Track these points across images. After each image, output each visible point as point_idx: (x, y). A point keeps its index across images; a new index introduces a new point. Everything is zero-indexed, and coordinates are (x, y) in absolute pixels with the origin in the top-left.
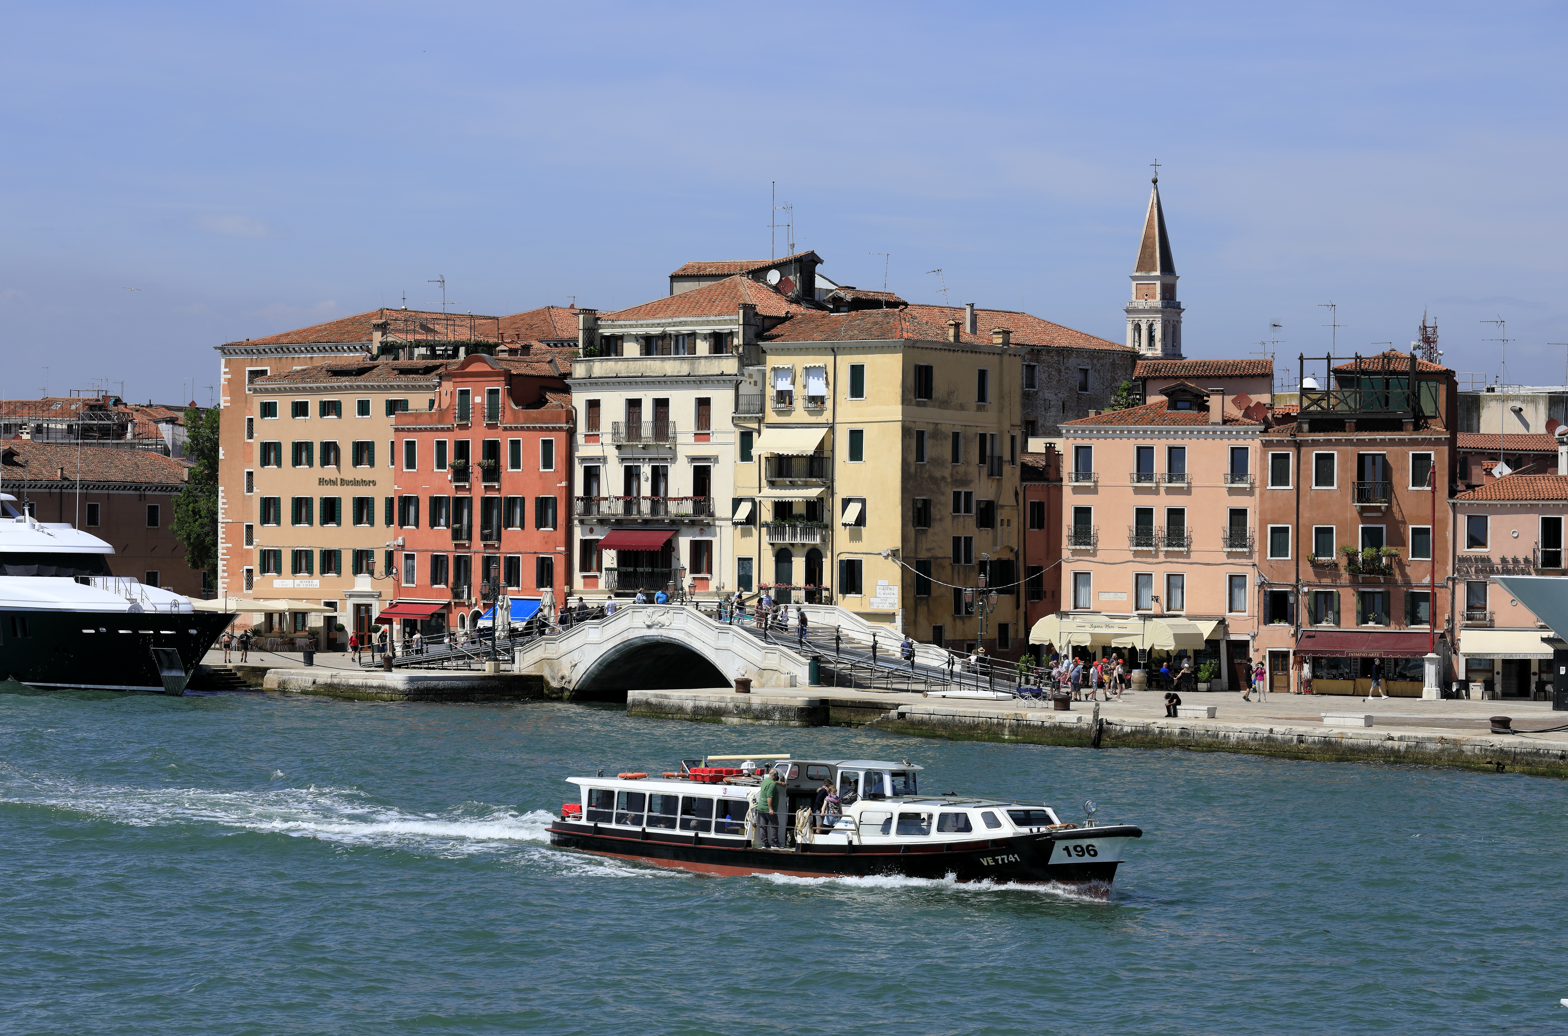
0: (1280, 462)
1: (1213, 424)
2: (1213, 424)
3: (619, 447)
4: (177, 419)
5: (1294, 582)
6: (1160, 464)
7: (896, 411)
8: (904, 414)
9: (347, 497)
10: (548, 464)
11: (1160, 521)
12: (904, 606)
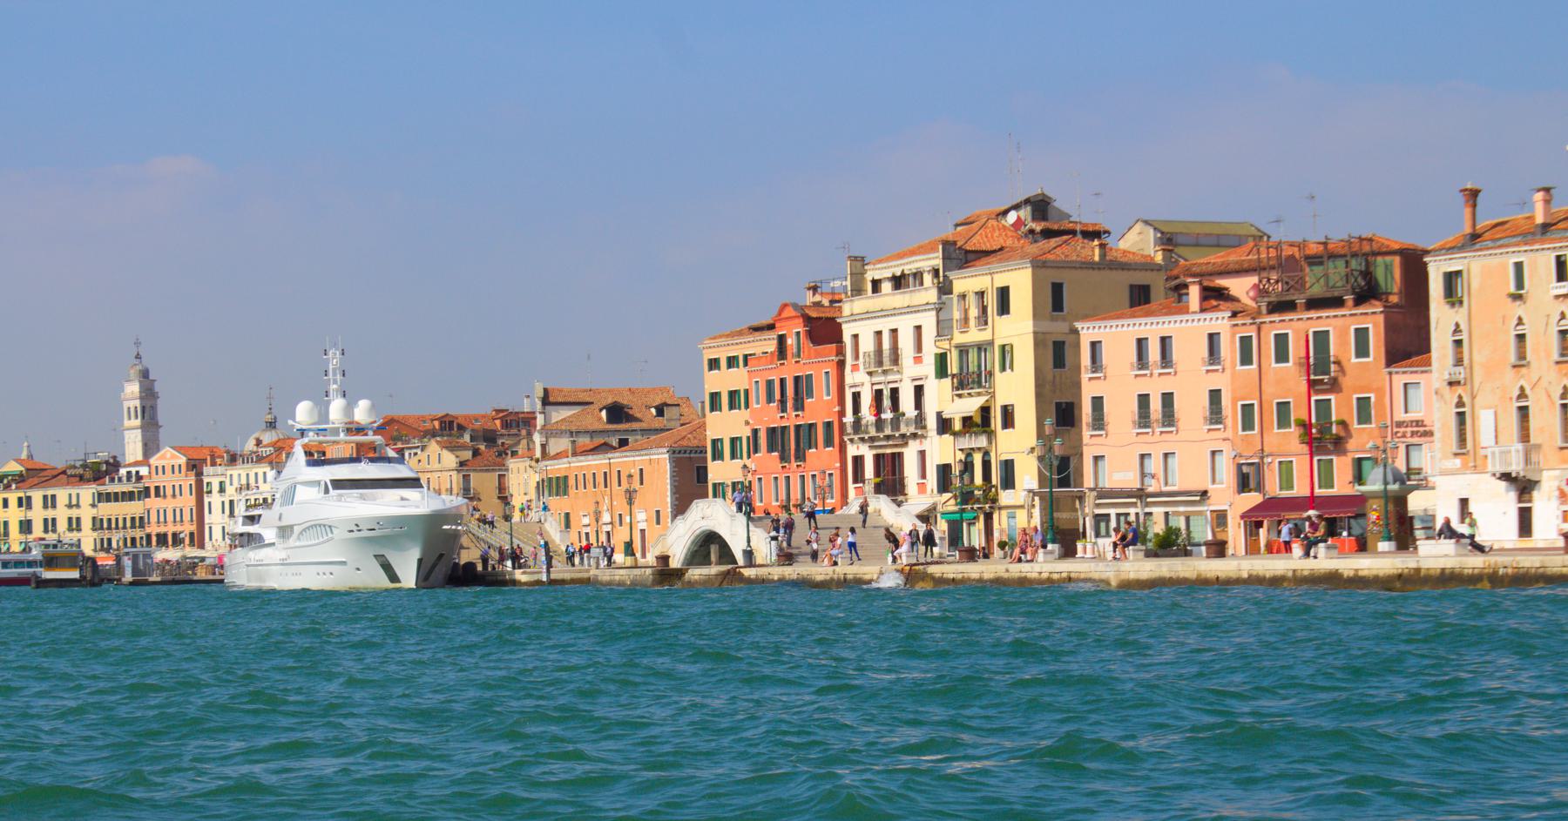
0: (1245, 342)
3: (870, 374)
11: (1156, 405)
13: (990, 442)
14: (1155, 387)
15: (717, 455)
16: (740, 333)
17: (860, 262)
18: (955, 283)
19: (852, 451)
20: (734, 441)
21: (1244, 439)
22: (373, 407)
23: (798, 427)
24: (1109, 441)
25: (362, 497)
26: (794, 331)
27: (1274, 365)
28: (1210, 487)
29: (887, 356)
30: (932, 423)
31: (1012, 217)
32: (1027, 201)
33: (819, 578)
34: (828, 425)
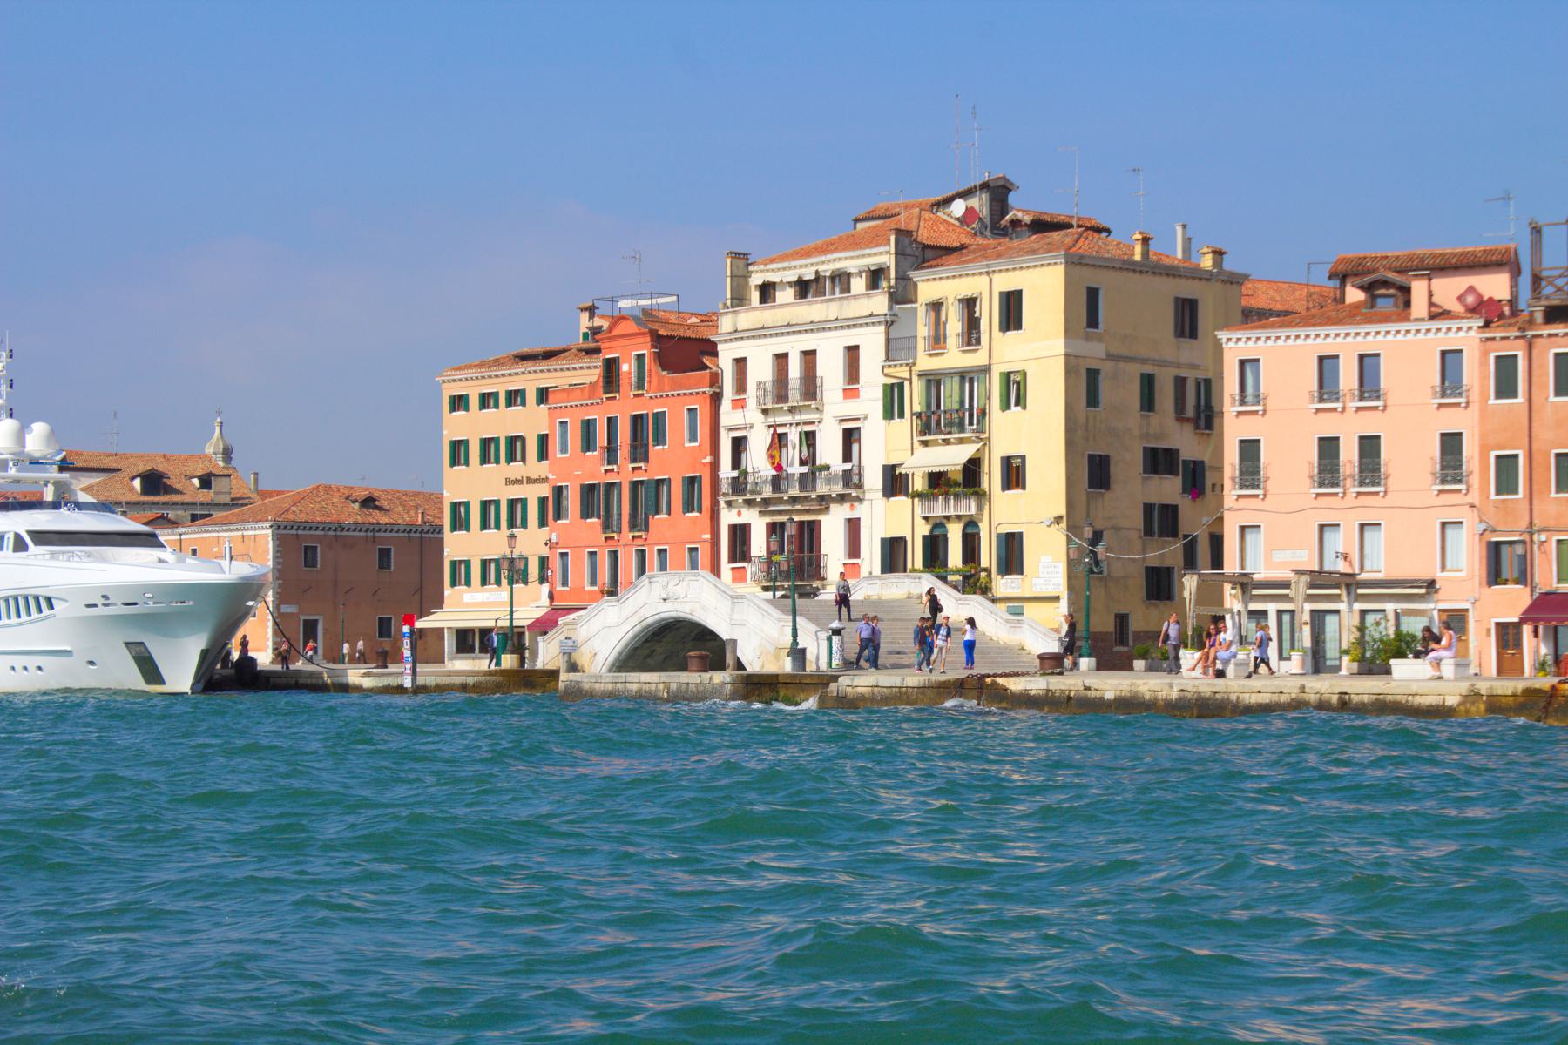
0: (1506, 367)
1: (1417, 320)
2: (1417, 320)
3: (765, 412)
5: (1524, 524)
6: (1348, 377)
7: (1058, 346)
8: (1067, 345)
9: (533, 494)
10: (693, 438)
11: (1349, 454)
12: (1071, 588)
13: (980, 508)
14: (1349, 428)
15: (460, 523)
16: (498, 363)
17: (742, 259)
18: (921, 286)
19: (728, 518)
20: (485, 505)
21: (1499, 506)
22: (53, 435)
23: (635, 485)
24: (1268, 504)
25: (89, 555)
26: (631, 354)
27: (1552, 398)
28: (1439, 575)
29: (795, 385)
30: (873, 480)
31: (958, 208)
32: (985, 186)
33: (1254, 699)
34: (691, 482)
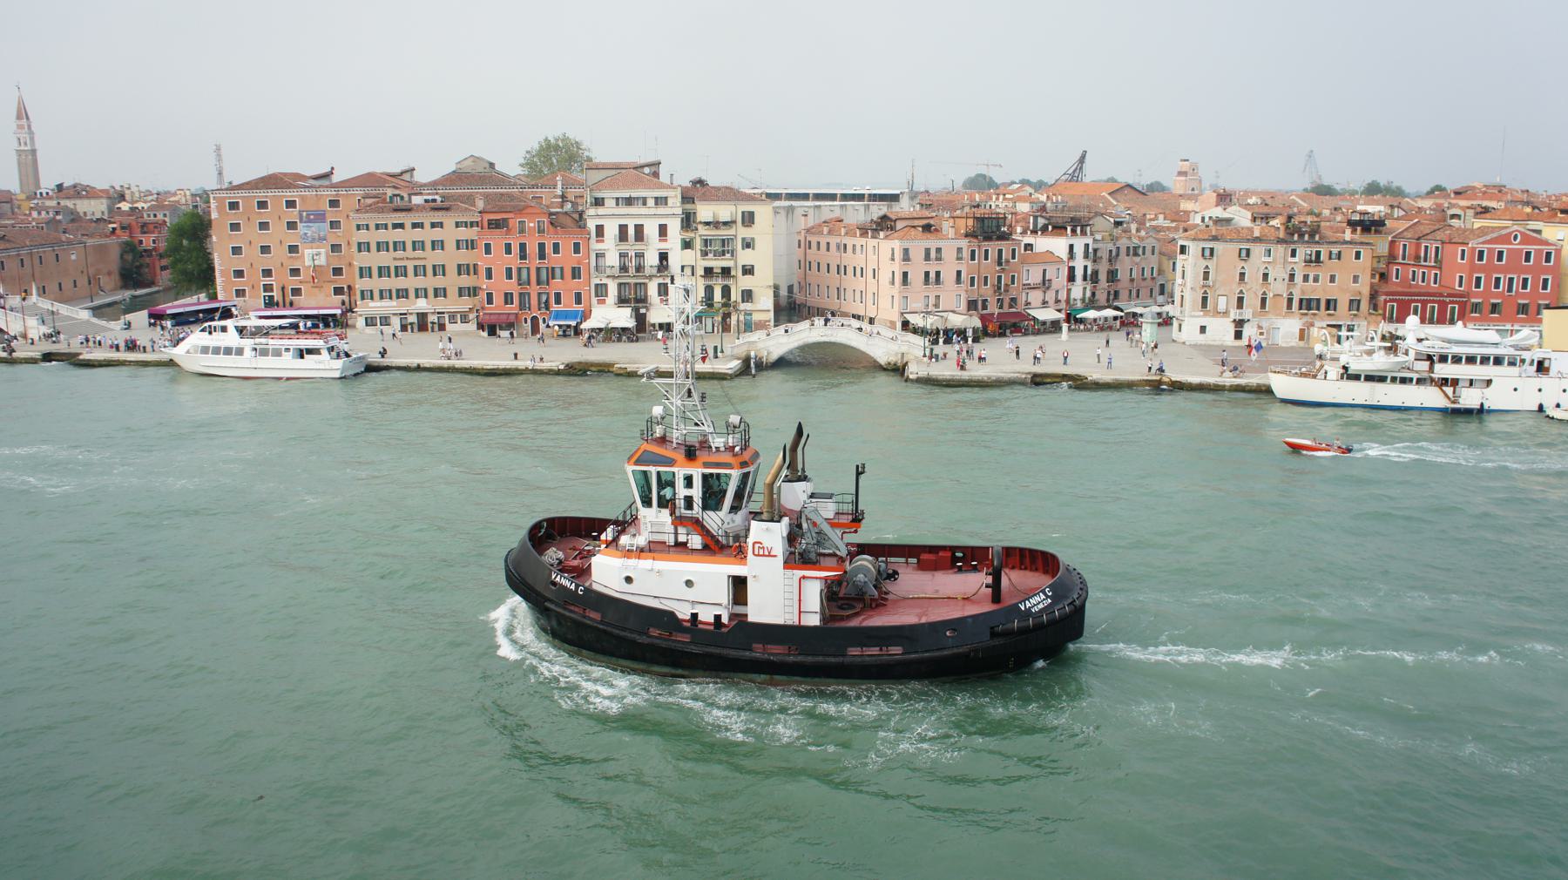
4: (1477, 214)
